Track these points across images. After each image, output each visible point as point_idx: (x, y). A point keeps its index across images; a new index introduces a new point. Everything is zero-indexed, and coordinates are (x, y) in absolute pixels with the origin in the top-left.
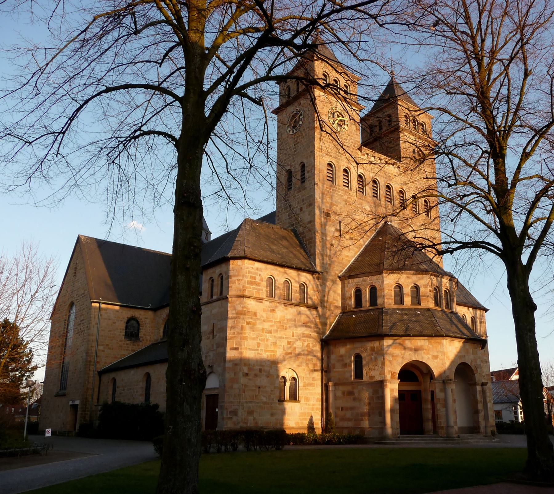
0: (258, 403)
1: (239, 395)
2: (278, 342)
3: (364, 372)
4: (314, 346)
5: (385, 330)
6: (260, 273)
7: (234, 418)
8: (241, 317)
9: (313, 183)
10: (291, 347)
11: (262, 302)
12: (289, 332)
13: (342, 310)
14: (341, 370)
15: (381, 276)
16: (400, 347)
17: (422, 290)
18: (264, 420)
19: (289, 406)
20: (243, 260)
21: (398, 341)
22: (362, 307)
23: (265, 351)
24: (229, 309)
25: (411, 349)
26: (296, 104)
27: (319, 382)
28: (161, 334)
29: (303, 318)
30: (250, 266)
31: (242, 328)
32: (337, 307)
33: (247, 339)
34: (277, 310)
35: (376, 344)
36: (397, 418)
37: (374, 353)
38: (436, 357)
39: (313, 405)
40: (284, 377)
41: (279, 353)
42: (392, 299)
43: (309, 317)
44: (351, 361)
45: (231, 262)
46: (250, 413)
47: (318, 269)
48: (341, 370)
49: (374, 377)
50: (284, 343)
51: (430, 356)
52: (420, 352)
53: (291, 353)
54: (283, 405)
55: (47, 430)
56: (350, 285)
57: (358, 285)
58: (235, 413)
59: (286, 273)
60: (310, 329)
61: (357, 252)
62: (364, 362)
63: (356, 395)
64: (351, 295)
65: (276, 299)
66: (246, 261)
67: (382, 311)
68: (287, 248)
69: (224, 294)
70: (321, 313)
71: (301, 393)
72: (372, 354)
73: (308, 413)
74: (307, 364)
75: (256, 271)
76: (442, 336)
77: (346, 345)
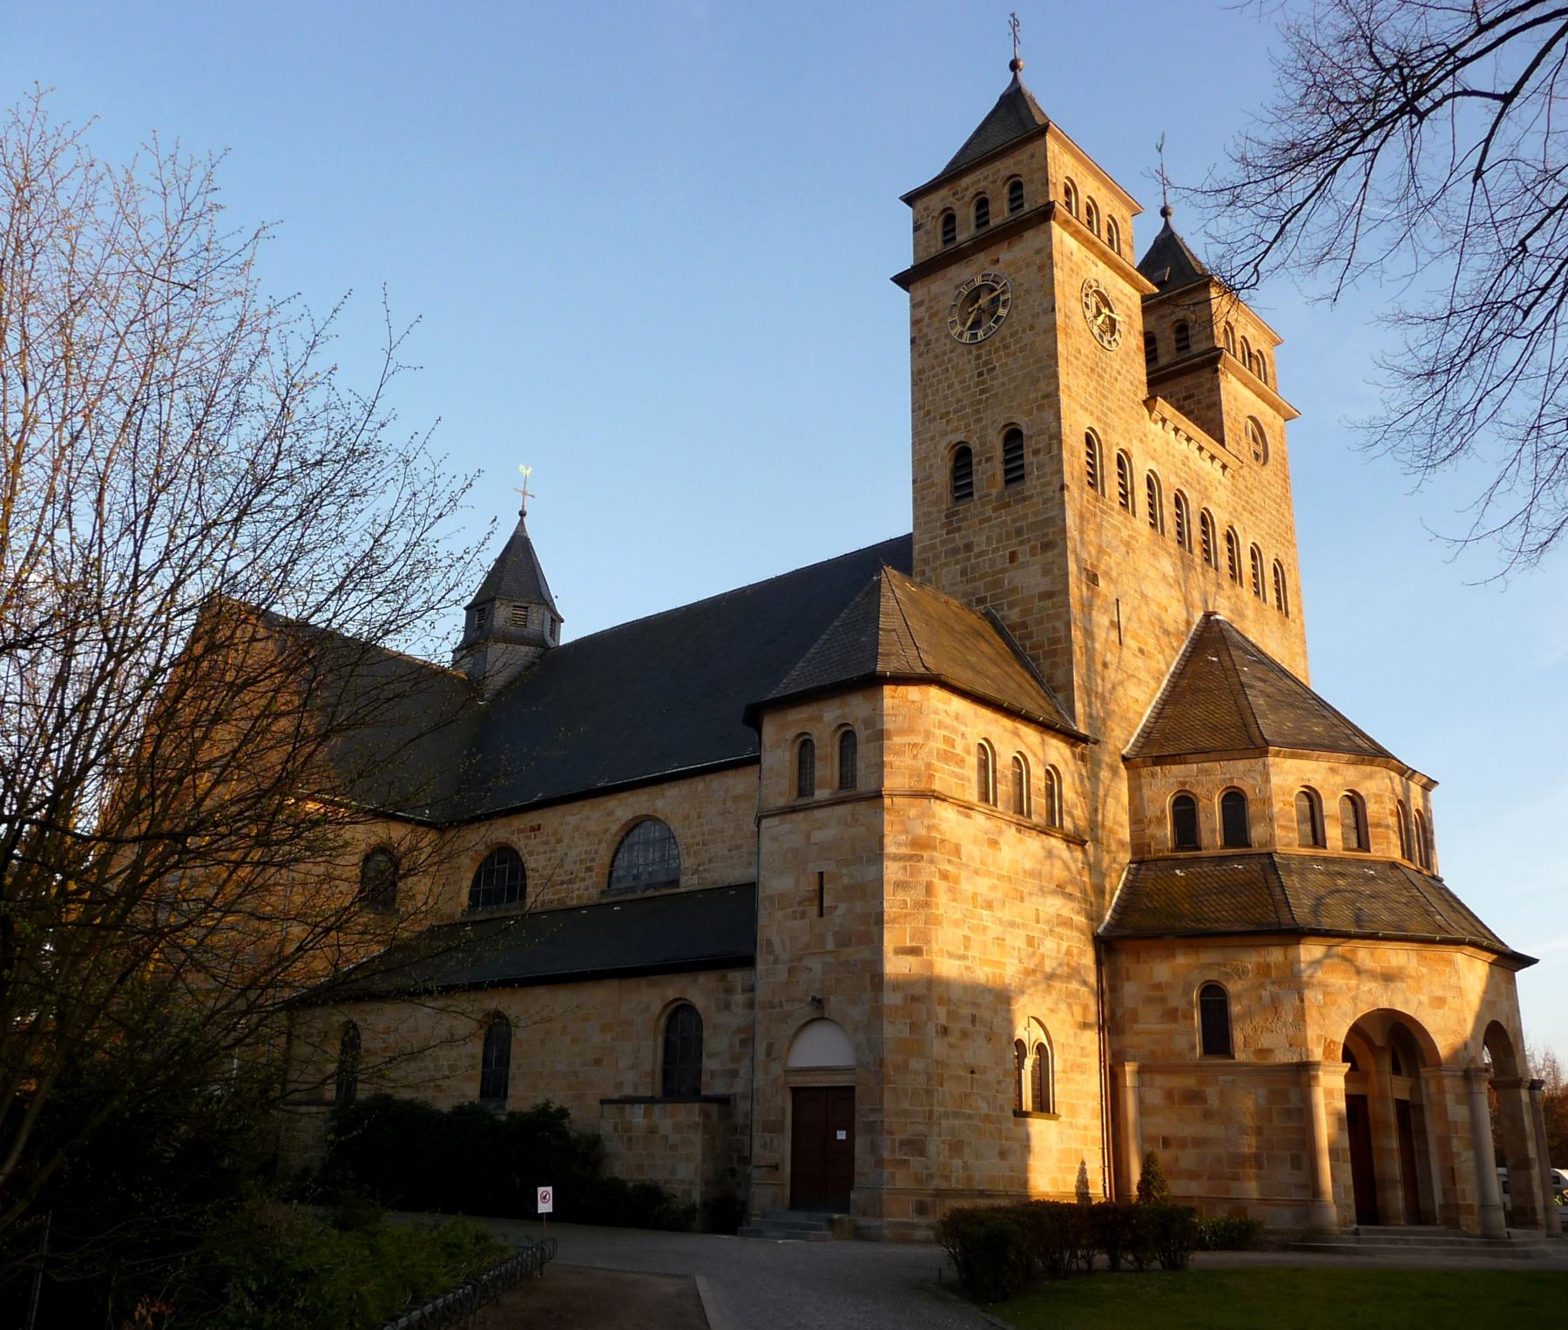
0: (970, 1117)
1: (929, 1092)
2: (1007, 937)
3: (1238, 1036)
4: (1081, 954)
5: (1302, 912)
6: (962, 728)
7: (916, 1162)
8: (926, 854)
9: (1058, 486)
10: (1034, 954)
11: (968, 816)
12: (1028, 908)
13: (1134, 853)
14: (1158, 1027)
15: (1257, 764)
16: (1344, 966)
17: (1372, 809)
18: (985, 1169)
19: (1038, 1127)
20: (924, 688)
21: (1339, 950)
22: (1200, 849)
23: (984, 962)
24: (887, 829)
25: (1373, 975)
26: (982, 258)
27: (1094, 1062)
28: (464, 898)
29: (1059, 873)
30: (941, 706)
31: (929, 889)
32: (1121, 844)
33: (940, 924)
34: (1001, 840)
35: (1275, 955)
36: (1347, 1168)
37: (1267, 981)
38: (1440, 1002)
39: (1086, 1128)
40: (1020, 1044)
41: (1010, 972)
42: (1292, 829)
43: (1069, 869)
44: (1190, 1003)
45: (888, 690)
46: (956, 1147)
47: (1082, 728)
48: (1158, 1027)
49: (1270, 1051)
50: (1017, 940)
51: (1424, 999)
52: (1399, 984)
53: (1034, 971)
54: (1025, 1125)
55: (540, 1190)
56: (1159, 782)
57: (1184, 784)
58: (917, 1146)
59: (1016, 734)
60: (1071, 904)
61: (1155, 692)
62: (1235, 1009)
63: (1213, 1101)
64: (1163, 811)
65: (1000, 807)
66: (934, 692)
67: (1269, 861)
68: (989, 664)
69: (864, 784)
70: (1091, 859)
71: (1060, 1091)
72: (1262, 985)
73: (1076, 1151)
74: (1070, 1006)
75: (955, 724)
76: (1458, 943)
77: (1173, 956)
